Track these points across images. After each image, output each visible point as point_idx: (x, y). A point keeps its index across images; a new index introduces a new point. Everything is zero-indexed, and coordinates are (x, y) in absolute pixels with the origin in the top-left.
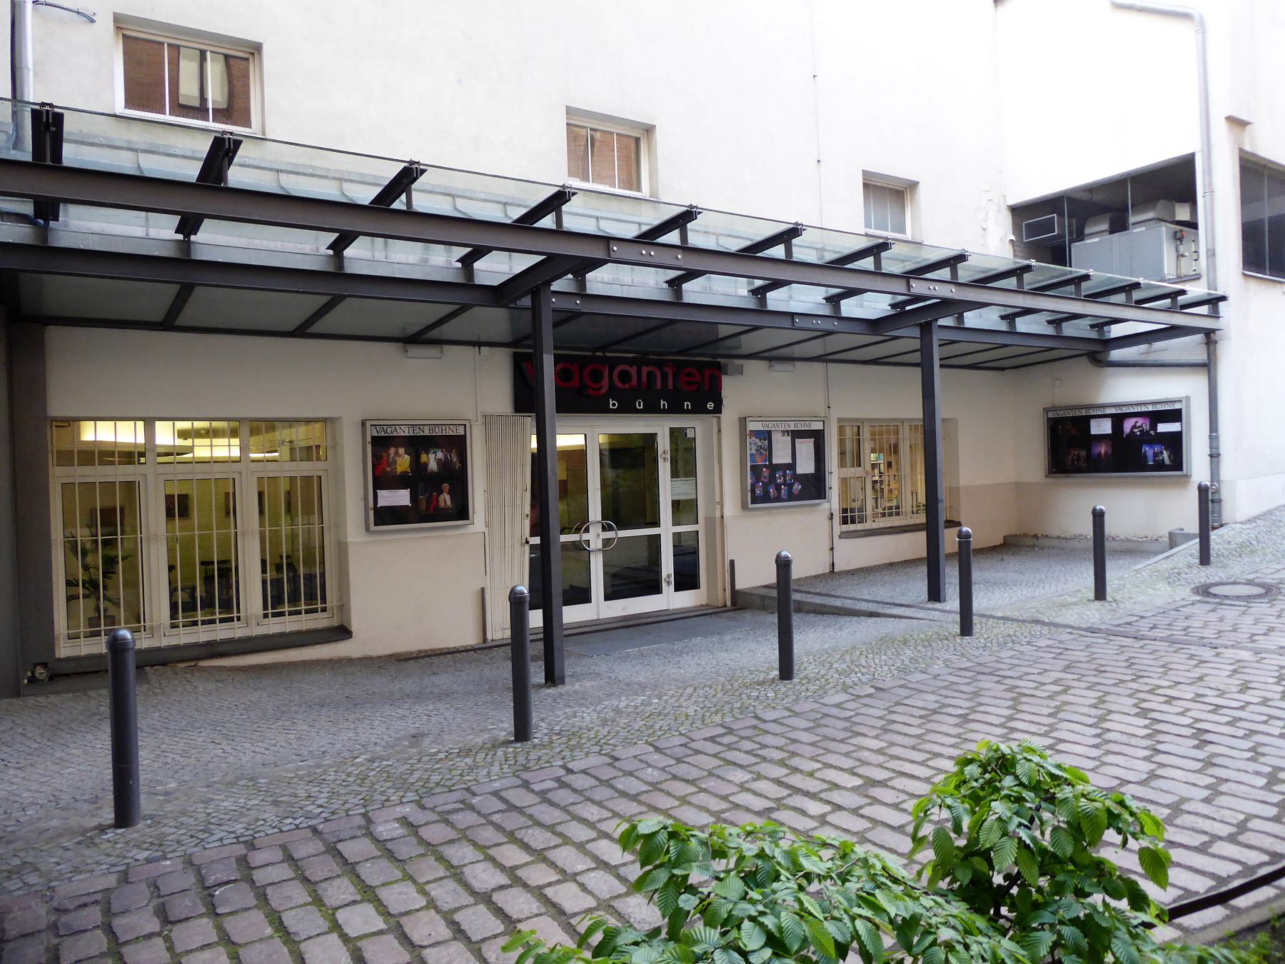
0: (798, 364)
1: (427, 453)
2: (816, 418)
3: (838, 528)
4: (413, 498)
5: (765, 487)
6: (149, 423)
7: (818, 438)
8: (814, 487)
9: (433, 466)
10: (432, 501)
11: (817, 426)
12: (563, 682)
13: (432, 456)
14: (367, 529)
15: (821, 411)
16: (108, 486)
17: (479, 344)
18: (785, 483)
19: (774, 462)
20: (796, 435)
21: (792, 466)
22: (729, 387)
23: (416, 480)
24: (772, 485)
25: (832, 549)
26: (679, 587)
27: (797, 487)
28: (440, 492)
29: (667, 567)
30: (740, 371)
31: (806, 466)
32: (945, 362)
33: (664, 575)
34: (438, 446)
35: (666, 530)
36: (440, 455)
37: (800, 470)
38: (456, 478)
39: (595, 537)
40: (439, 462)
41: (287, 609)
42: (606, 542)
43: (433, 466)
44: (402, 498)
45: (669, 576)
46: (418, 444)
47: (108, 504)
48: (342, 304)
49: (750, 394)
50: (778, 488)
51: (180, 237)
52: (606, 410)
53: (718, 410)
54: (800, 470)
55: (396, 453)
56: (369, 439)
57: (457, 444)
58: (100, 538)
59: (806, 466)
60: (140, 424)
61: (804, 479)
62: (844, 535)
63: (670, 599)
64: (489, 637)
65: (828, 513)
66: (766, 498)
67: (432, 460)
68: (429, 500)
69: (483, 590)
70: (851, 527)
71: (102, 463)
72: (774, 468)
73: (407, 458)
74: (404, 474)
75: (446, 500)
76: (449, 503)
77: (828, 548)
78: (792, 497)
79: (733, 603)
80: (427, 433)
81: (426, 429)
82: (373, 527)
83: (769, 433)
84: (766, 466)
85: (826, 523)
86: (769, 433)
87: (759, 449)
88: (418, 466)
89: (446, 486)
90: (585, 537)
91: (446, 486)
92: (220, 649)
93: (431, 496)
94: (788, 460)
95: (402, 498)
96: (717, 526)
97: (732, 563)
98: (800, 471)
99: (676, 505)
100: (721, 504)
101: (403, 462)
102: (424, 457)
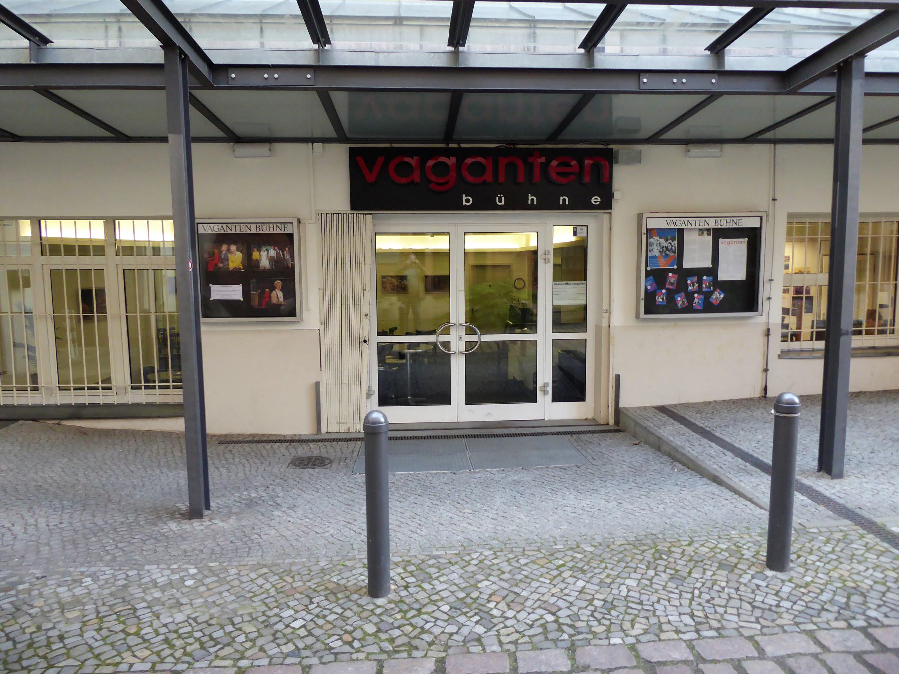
0: (728, 147)
1: (259, 250)
2: (750, 212)
3: (777, 345)
4: (245, 293)
5: (671, 295)
6: (111, 223)
7: (753, 237)
8: (744, 296)
9: (265, 263)
10: (265, 297)
11: (754, 223)
12: (840, 476)
13: (264, 254)
14: (638, 316)
15: (763, 203)
16: (86, 273)
17: (312, 140)
18: (700, 291)
19: (687, 265)
20: (718, 234)
21: (712, 272)
22: (624, 178)
23: (248, 275)
24: (671, 290)
25: (766, 370)
26: (558, 397)
27: (718, 296)
28: (273, 288)
29: (545, 375)
30: (637, 159)
31: (733, 267)
32: (871, 135)
33: (540, 384)
34: (270, 244)
35: (545, 338)
36: (272, 252)
37: (724, 275)
38: (285, 273)
39: (457, 340)
40: (271, 259)
41: (171, 384)
42: (469, 345)
43: (265, 263)
44: (235, 292)
45: (546, 385)
46: (250, 242)
47: (86, 286)
48: (720, 99)
49: (647, 187)
50: (690, 296)
51: (451, 49)
52: (459, 207)
53: (607, 204)
54: (724, 275)
55: (228, 250)
56: (644, 231)
57: (285, 241)
58: (138, 314)
59: (733, 267)
60: (101, 223)
61: (729, 286)
62: (785, 355)
63: (545, 409)
64: (324, 429)
65: (764, 328)
66: (671, 308)
67: (264, 257)
68: (261, 296)
69: (317, 385)
70: (794, 345)
71: (139, 254)
72: (684, 273)
73: (239, 255)
74: (236, 271)
75: (278, 295)
76: (281, 299)
77: (761, 367)
78: (708, 307)
79: (617, 422)
80: (254, 231)
81: (253, 227)
82: (643, 315)
83: (681, 231)
84: (672, 270)
85: (760, 340)
86: (681, 231)
87: (664, 250)
88: (250, 264)
89: (278, 283)
90: (443, 338)
91: (278, 283)
92: (85, 412)
93: (263, 291)
94: (708, 264)
95: (235, 292)
96: (605, 334)
97: (618, 378)
98: (723, 276)
99: (557, 312)
100: (608, 311)
101: (235, 259)
102: (255, 255)
